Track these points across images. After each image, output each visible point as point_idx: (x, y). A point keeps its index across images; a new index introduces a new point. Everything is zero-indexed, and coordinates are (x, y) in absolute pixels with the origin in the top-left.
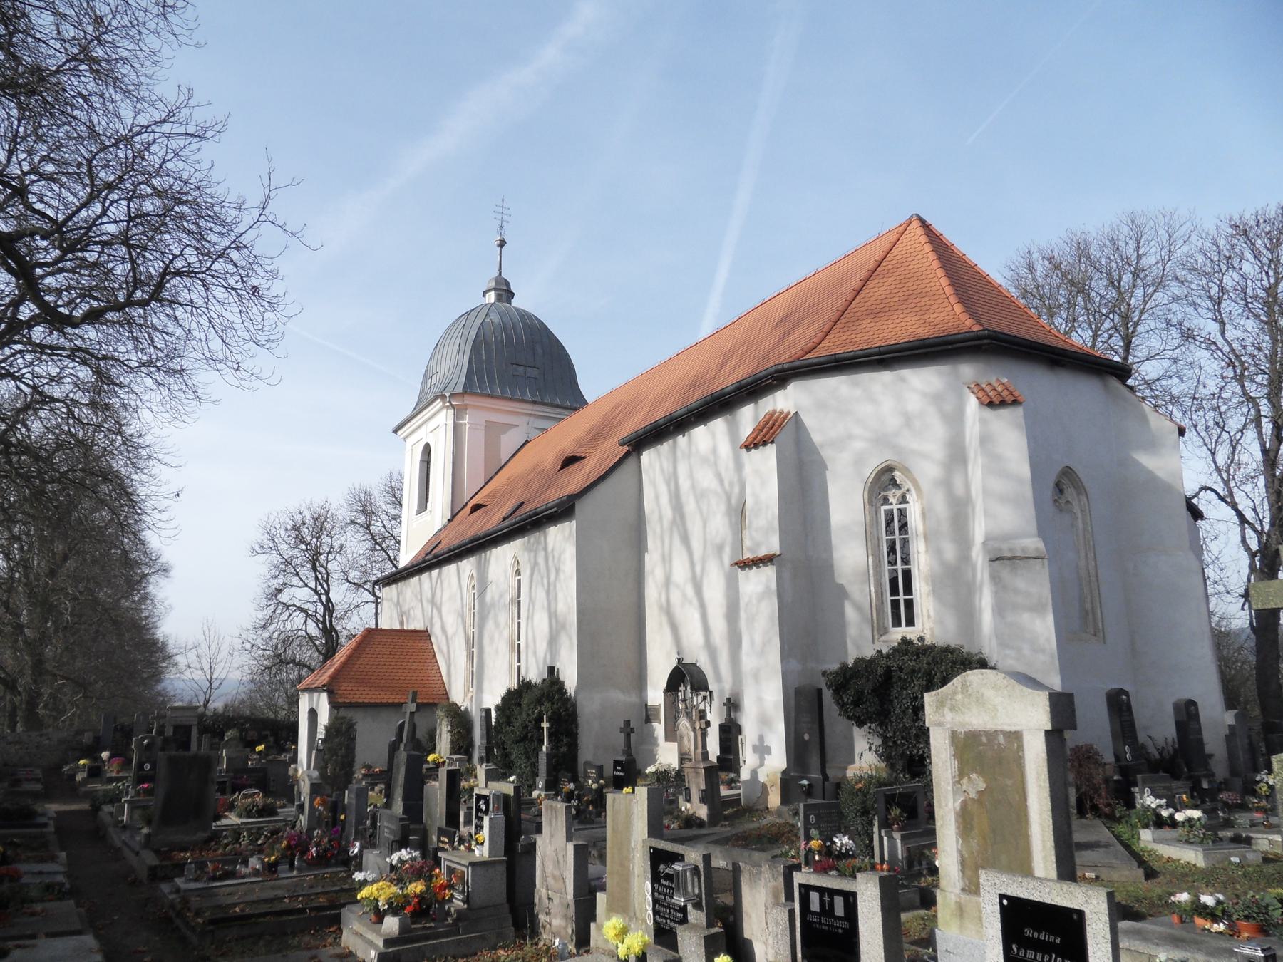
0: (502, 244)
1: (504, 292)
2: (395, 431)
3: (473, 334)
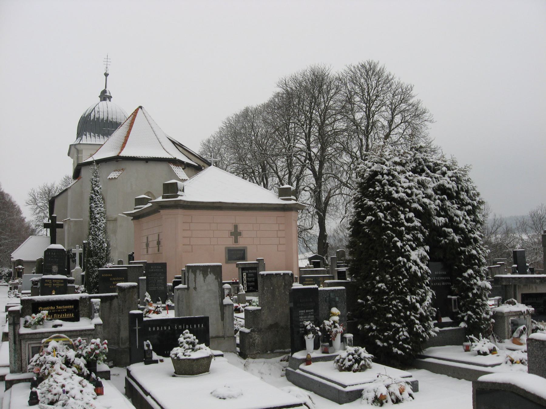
0: (106, 75)
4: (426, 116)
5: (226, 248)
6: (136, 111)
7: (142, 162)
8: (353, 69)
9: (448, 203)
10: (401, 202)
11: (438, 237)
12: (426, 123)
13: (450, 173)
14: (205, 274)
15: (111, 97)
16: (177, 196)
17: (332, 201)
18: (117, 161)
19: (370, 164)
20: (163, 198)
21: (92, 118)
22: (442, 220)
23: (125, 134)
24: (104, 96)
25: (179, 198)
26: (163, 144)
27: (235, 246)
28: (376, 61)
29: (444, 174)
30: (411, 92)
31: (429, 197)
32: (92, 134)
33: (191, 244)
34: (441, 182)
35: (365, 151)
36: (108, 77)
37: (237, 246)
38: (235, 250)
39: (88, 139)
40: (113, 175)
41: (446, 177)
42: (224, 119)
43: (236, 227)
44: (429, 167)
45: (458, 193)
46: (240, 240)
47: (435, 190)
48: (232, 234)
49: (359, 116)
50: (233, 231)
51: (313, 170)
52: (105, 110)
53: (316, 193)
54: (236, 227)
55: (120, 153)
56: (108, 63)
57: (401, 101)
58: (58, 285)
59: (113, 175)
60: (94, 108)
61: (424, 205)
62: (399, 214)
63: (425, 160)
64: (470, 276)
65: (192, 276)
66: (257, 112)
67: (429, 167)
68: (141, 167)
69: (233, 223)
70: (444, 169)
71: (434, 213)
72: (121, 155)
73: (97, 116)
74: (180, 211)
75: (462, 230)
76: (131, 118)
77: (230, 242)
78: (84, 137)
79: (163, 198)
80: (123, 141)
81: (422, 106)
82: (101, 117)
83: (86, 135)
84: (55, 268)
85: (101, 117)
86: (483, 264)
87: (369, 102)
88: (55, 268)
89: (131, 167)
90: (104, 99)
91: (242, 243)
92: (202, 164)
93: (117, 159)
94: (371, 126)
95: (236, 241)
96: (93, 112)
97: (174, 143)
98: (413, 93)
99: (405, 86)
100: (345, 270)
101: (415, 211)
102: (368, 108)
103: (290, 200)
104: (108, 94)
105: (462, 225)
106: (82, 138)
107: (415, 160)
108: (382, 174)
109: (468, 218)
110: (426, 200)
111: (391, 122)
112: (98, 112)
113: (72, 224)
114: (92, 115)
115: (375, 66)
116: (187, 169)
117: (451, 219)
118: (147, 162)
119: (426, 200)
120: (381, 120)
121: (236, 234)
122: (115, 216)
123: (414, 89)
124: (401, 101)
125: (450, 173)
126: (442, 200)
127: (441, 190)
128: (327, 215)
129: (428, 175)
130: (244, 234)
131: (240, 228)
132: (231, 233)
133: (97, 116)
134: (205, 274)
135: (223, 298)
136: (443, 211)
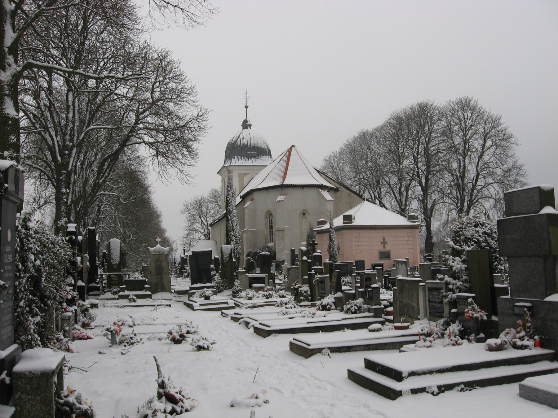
0: (246, 107)
4: (512, 140)
5: (379, 251)
6: (290, 150)
7: (299, 188)
8: (451, 104)
9: (487, 238)
10: (470, 239)
12: (512, 145)
13: (489, 226)
14: (402, 265)
15: (251, 125)
16: (351, 223)
17: (437, 207)
18: (282, 188)
19: (458, 224)
21: (238, 144)
22: (485, 244)
23: (284, 167)
24: (246, 125)
25: (353, 224)
26: (312, 173)
28: (470, 97)
29: (486, 227)
30: (500, 121)
31: (480, 236)
32: (239, 157)
34: (485, 230)
36: (248, 109)
39: (236, 162)
40: (280, 198)
41: (487, 229)
42: (345, 141)
43: (384, 239)
44: (481, 224)
45: (491, 234)
46: (386, 246)
47: (483, 233)
49: (458, 140)
51: (420, 183)
52: (248, 137)
53: (423, 201)
54: (384, 239)
55: (283, 182)
56: (248, 97)
57: (492, 128)
58: (319, 271)
59: (280, 198)
60: (239, 136)
61: (478, 239)
63: (479, 222)
64: (496, 265)
65: (398, 265)
66: (372, 135)
67: (481, 224)
68: (299, 192)
70: (487, 225)
71: (482, 242)
72: (285, 183)
73: (242, 142)
74: (354, 231)
75: (493, 247)
76: (287, 154)
77: (381, 248)
78: (233, 160)
80: (283, 172)
81: (509, 131)
82: (246, 143)
83: (234, 158)
84: (318, 263)
85: (246, 143)
86: (502, 260)
87: (465, 131)
88: (318, 263)
89: (291, 191)
90: (246, 128)
91: (388, 248)
92: (339, 186)
93: (282, 187)
94: (467, 150)
95: (384, 247)
96: (239, 139)
97: (318, 171)
98: (502, 121)
99: (494, 116)
100: (264, 276)
101: (474, 241)
102: (465, 135)
103: (415, 222)
104: (249, 123)
105: (493, 246)
106: (231, 161)
107: (475, 222)
108: (463, 228)
109: (495, 243)
110: (479, 238)
111: (483, 146)
112: (243, 139)
113: (249, 233)
114: (238, 142)
115: (469, 102)
116: (331, 192)
117: (489, 244)
118: (303, 188)
119: (479, 238)
120: (476, 144)
121: (384, 243)
122: (283, 227)
123: (502, 118)
124: (492, 128)
125: (489, 226)
126: (485, 237)
127: (485, 233)
128: (432, 218)
129: (480, 228)
130: (389, 243)
131: (386, 240)
133: (242, 142)
134: (402, 265)
135: (407, 272)
136: (485, 241)
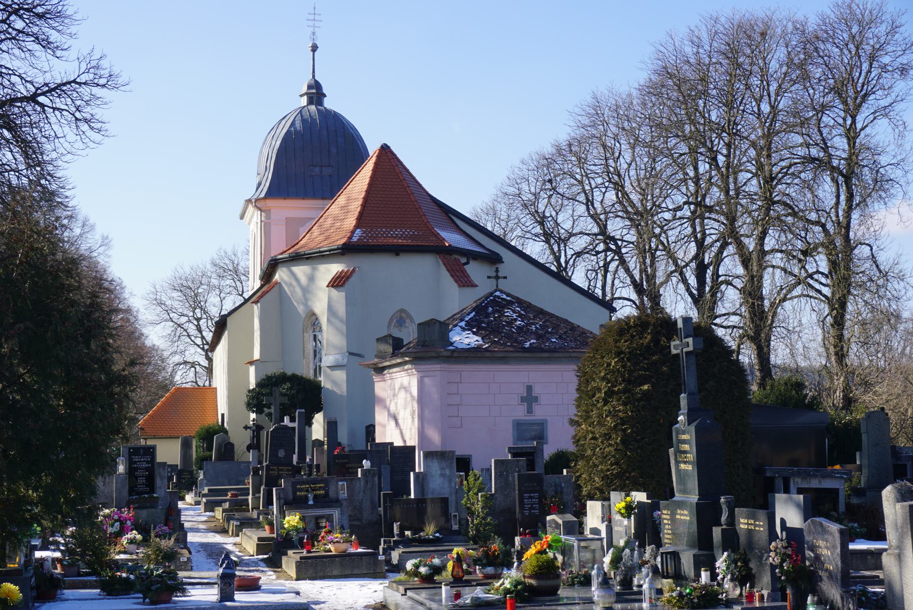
0: (314, 48)
1: (316, 93)
2: (242, 217)
3: (279, 143)
5: (514, 421)
11: (119, 573)
20: (380, 507)
27: (528, 418)
33: (460, 415)
35: (674, 346)
37: (531, 418)
38: (529, 424)
43: (529, 388)
48: (523, 400)
50: (525, 395)
54: (529, 388)
62: (361, 544)
69: (524, 383)
77: (520, 413)
79: (380, 507)
91: (539, 413)
95: (530, 411)
121: (529, 399)
130: (543, 400)
131: (536, 391)
132: (522, 397)
